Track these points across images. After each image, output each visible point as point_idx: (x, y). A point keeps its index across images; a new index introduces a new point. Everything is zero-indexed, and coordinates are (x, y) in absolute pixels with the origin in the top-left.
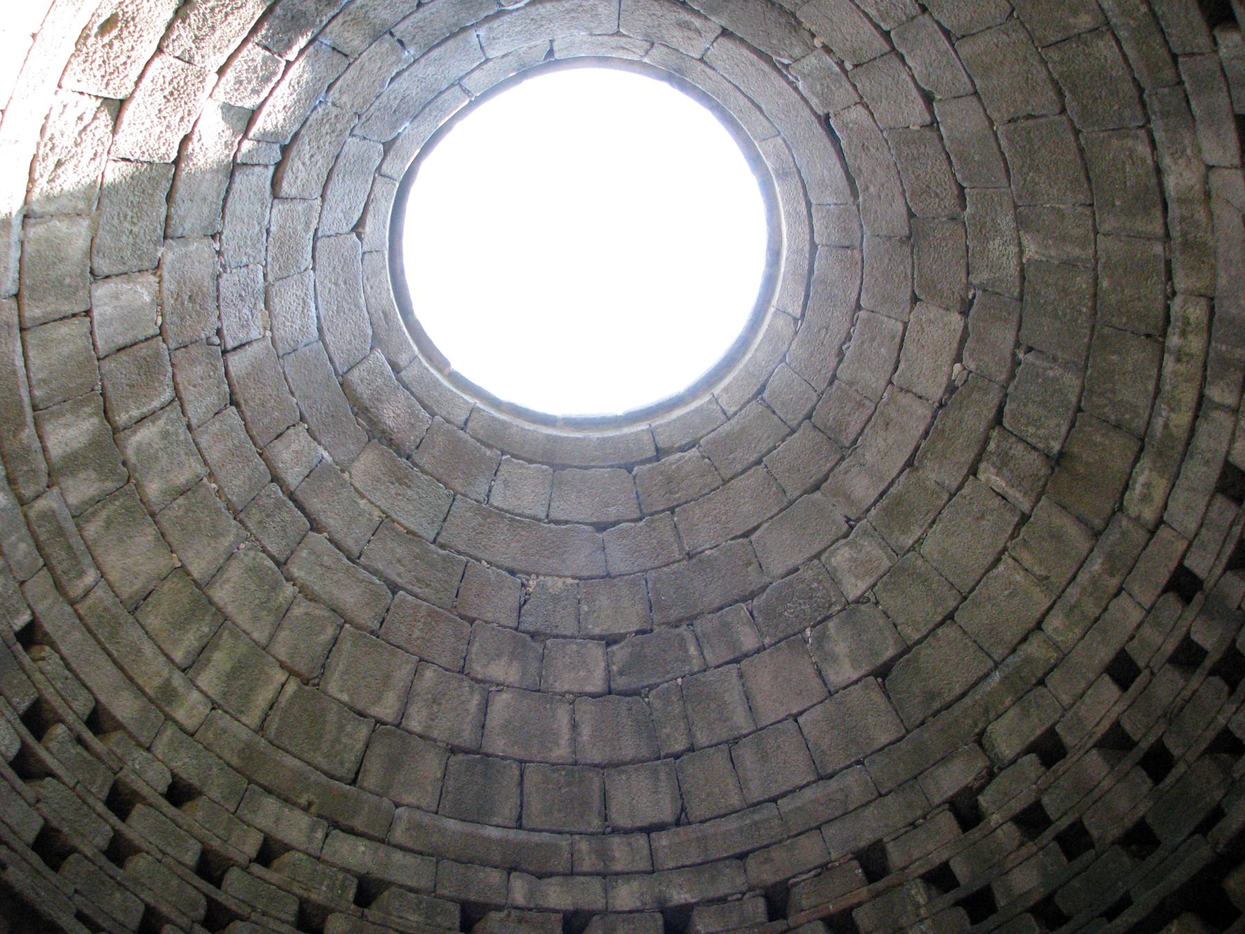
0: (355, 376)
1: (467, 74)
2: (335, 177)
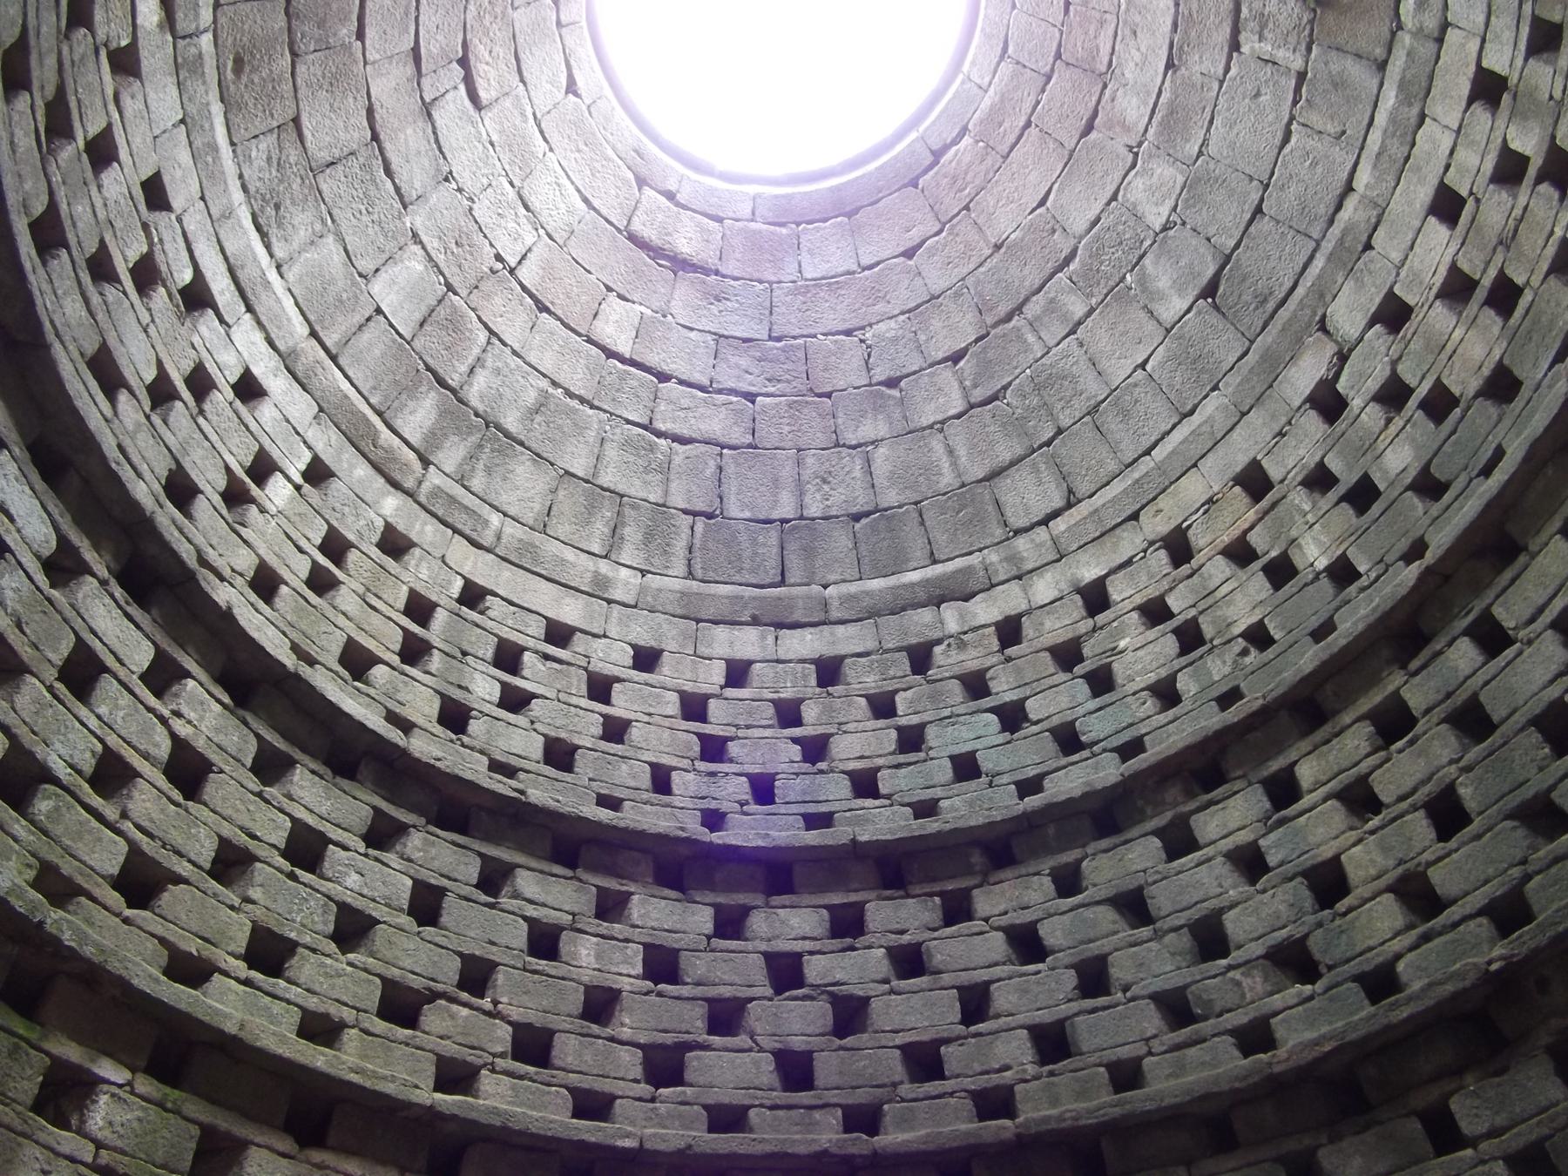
0: (636, 226)
2: (522, 56)
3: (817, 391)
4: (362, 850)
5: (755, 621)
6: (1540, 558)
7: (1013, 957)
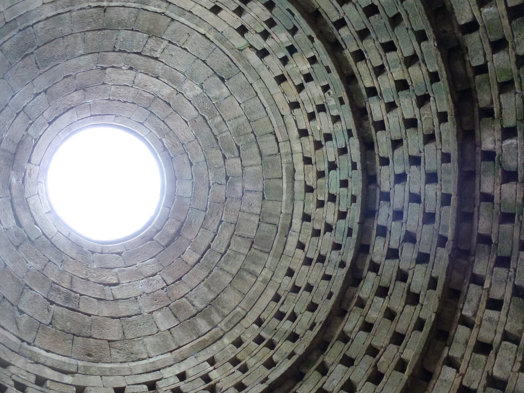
0: (163, 244)
1: (64, 236)
2: (107, 267)
4: (327, 377)
5: (286, 236)
6: (321, 6)
7: (404, 183)
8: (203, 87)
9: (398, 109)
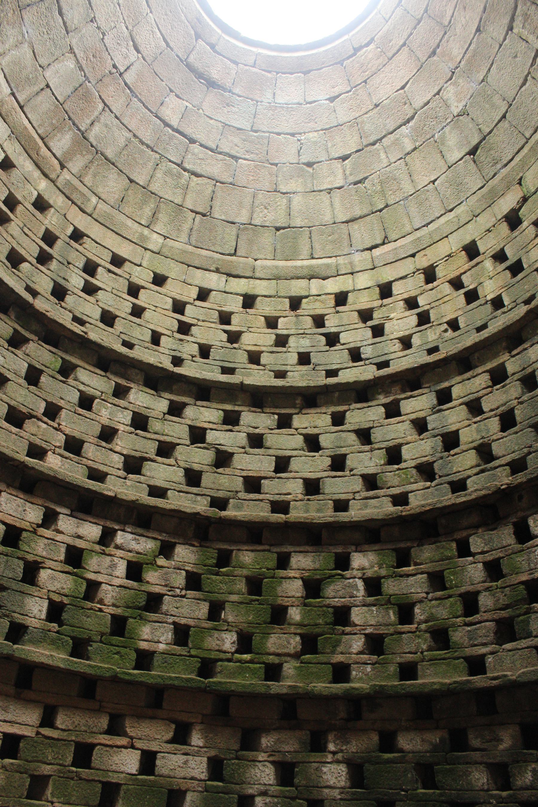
3: (270, 162)
4: (6, 347)
5: (217, 271)
8: (461, 115)
9: (417, 437)
